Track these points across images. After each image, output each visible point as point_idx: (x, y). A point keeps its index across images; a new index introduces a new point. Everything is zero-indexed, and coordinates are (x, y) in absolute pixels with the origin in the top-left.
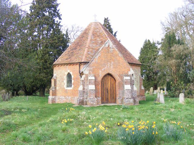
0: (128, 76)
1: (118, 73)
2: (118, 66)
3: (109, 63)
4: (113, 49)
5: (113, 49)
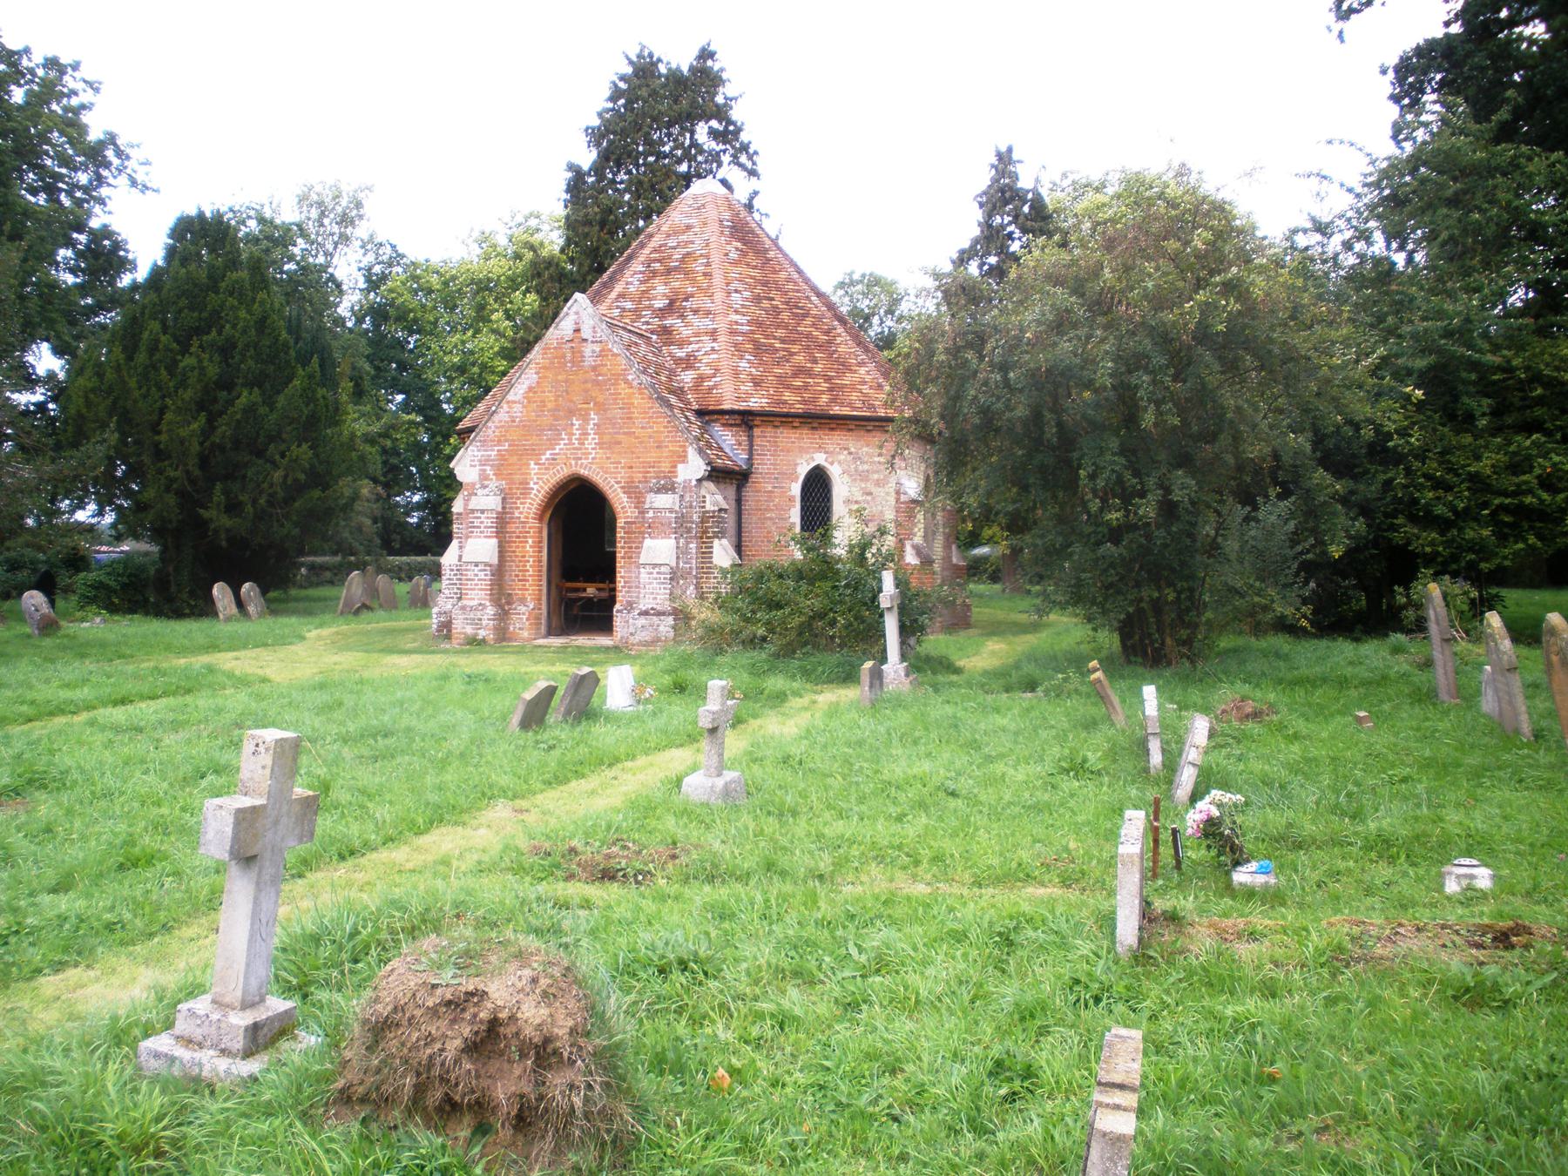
0: (669, 488)
1: (623, 475)
2: (620, 438)
3: (577, 423)
4: (597, 348)
5: (597, 348)
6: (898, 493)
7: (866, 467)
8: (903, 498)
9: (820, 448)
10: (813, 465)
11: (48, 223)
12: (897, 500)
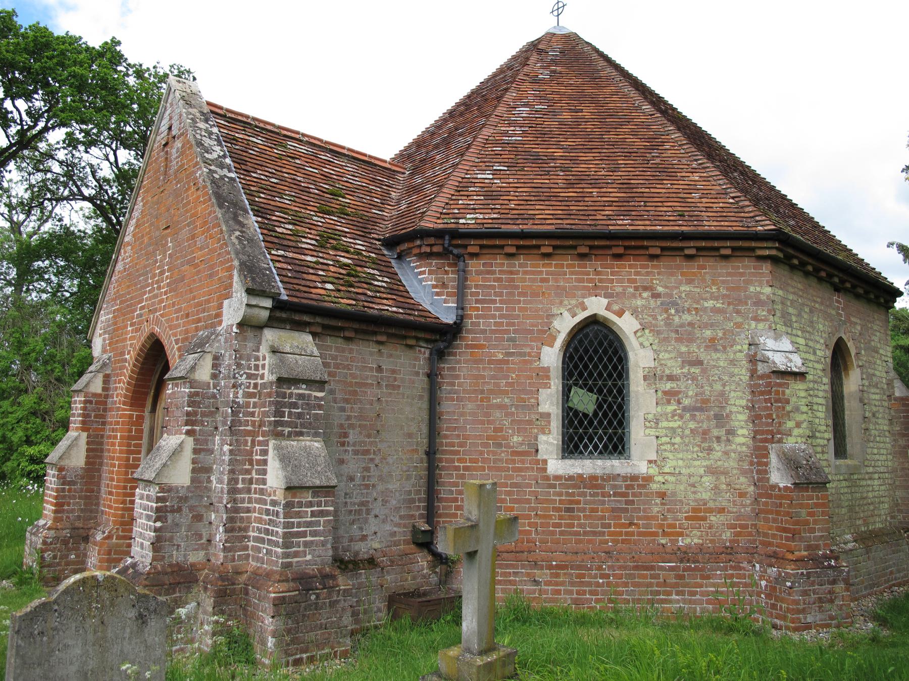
6: (753, 360)
7: (687, 318)
8: (761, 369)
9: (595, 291)
10: (582, 316)
11: (685, 553)
12: (753, 373)
